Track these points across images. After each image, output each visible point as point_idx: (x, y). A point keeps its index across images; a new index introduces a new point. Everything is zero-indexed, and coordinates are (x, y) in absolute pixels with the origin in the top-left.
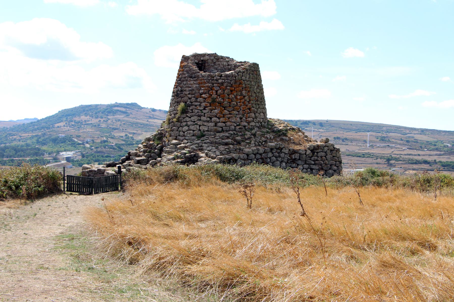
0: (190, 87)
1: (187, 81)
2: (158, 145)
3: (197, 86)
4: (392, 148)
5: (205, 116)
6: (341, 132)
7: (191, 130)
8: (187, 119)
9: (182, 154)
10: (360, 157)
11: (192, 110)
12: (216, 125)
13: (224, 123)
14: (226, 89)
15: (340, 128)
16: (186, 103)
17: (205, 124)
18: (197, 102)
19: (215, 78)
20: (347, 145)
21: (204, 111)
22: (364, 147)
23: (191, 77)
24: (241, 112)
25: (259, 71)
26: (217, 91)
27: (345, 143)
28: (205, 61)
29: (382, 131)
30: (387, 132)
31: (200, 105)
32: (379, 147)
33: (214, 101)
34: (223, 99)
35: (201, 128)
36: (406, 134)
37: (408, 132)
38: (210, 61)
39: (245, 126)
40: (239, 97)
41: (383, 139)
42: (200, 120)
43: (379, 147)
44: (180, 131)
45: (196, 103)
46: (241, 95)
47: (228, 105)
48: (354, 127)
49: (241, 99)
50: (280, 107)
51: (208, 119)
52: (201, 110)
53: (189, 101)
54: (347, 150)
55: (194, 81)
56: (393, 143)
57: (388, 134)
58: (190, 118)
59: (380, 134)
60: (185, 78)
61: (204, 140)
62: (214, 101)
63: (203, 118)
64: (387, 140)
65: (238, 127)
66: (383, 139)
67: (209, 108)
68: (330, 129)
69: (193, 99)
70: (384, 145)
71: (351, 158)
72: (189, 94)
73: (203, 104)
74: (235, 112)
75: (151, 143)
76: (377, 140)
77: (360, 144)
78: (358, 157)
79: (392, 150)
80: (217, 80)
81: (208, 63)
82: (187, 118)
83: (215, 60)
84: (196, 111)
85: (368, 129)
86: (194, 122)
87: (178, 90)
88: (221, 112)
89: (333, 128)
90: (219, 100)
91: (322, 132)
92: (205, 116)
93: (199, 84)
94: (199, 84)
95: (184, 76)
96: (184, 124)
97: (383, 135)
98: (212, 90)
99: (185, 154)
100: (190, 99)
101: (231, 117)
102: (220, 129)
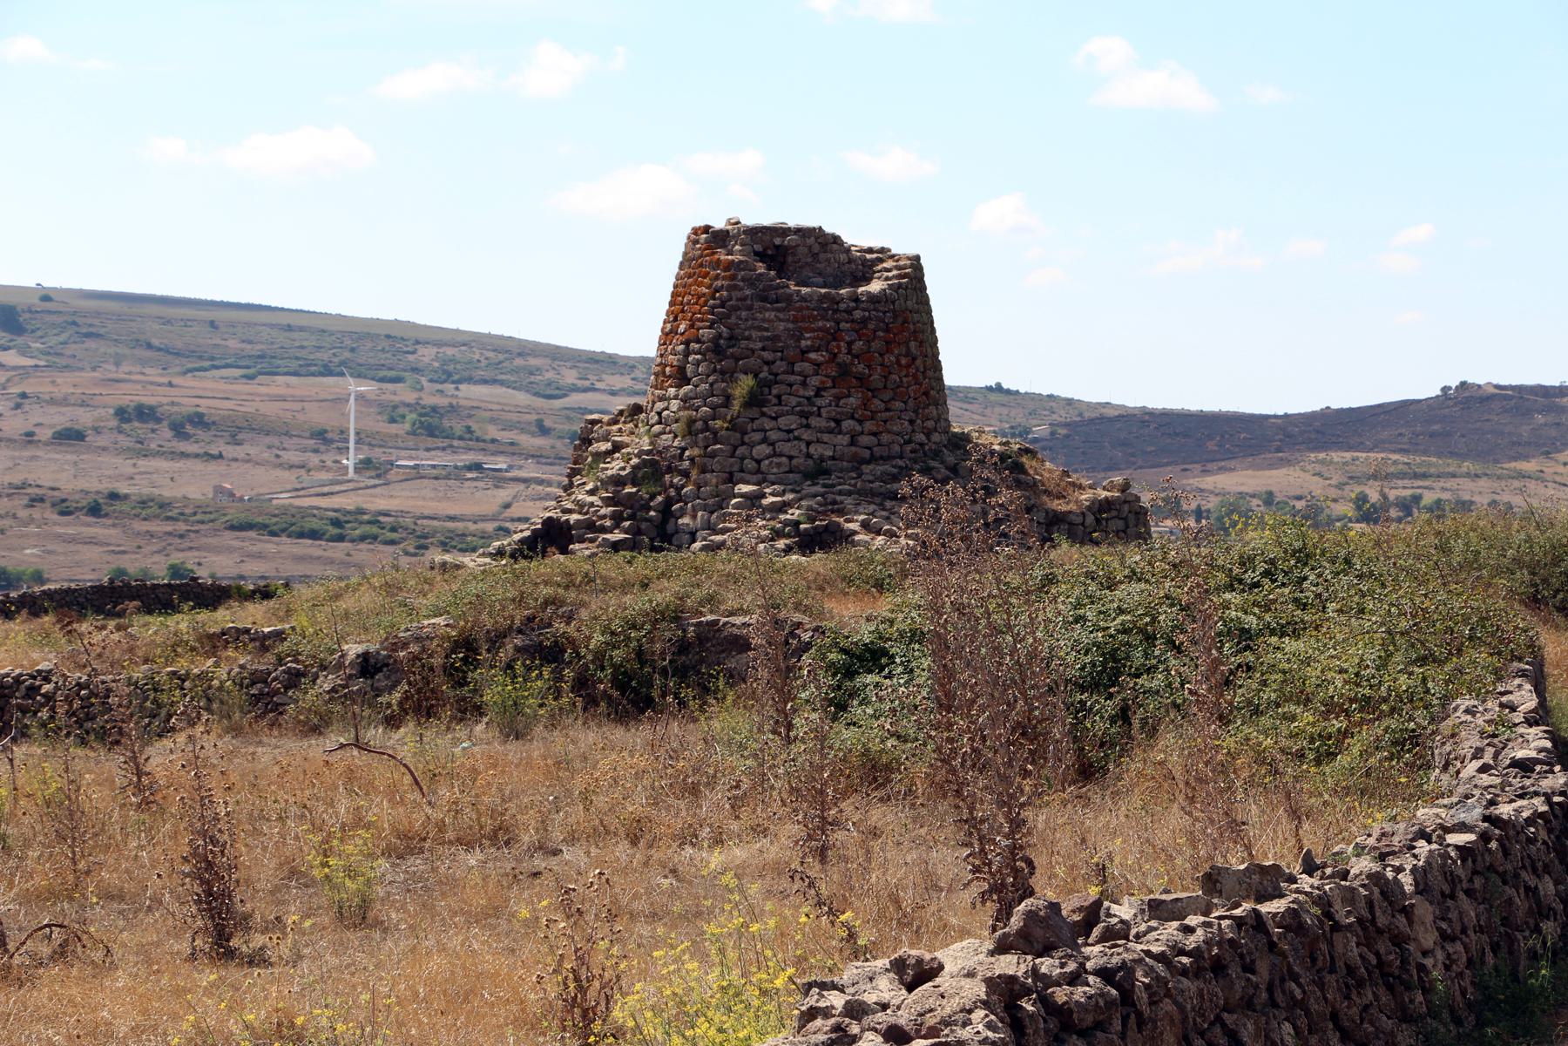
0: (767, 330)
1: (750, 308)
2: (653, 497)
3: (791, 326)
4: (499, 478)
5: (819, 415)
6: (153, 374)
7: (781, 455)
8: (768, 424)
9: (786, 523)
10: (314, 535)
11: (779, 397)
12: (853, 443)
13: (875, 434)
14: (875, 337)
15: (137, 343)
16: (756, 376)
17: (826, 437)
18: (793, 373)
19: (843, 306)
20: (213, 457)
21: (819, 402)
22: (324, 476)
23: (765, 299)
24: (911, 403)
26: (850, 344)
27: (192, 448)
28: (787, 248)
29: (415, 370)
30: (447, 374)
31: (804, 384)
32: (417, 474)
33: (844, 371)
34: (869, 367)
35: (812, 450)
36: (563, 392)
37: (570, 377)
38: (802, 250)
39: (922, 445)
40: (904, 361)
41: (432, 426)
42: (808, 426)
43: (417, 474)
44: (743, 459)
45: (792, 378)
46: (908, 354)
47: (881, 385)
48: (233, 344)
49: (908, 366)
50: (979, 348)
51: (833, 424)
52: (808, 399)
53: (766, 368)
54: (219, 490)
55: (778, 310)
56: (496, 448)
57: (449, 387)
58: (775, 419)
60: (743, 299)
61: (833, 486)
62: (844, 371)
63: (814, 421)
64: (458, 429)
65: (908, 448)
66: (432, 426)
67: (834, 391)
68: (71, 349)
69: (780, 366)
71: (259, 547)
72: (763, 349)
73: (814, 381)
74: (899, 405)
75: (629, 490)
76: (394, 429)
77: (292, 456)
78: (301, 535)
79: (504, 495)
80: (849, 312)
81: (794, 254)
82: (765, 420)
83: (816, 248)
84: (793, 401)
85: (325, 356)
86: (789, 431)
87: (720, 336)
88: (865, 405)
89: (91, 344)
90: (804, 343)
91: (24, 373)
92: (819, 415)
93: (795, 320)
94: (795, 320)
95: (735, 294)
96: (758, 436)
97: (429, 400)
98: (835, 339)
99: (797, 523)
100: (767, 363)
101: (891, 418)
102: (867, 454)
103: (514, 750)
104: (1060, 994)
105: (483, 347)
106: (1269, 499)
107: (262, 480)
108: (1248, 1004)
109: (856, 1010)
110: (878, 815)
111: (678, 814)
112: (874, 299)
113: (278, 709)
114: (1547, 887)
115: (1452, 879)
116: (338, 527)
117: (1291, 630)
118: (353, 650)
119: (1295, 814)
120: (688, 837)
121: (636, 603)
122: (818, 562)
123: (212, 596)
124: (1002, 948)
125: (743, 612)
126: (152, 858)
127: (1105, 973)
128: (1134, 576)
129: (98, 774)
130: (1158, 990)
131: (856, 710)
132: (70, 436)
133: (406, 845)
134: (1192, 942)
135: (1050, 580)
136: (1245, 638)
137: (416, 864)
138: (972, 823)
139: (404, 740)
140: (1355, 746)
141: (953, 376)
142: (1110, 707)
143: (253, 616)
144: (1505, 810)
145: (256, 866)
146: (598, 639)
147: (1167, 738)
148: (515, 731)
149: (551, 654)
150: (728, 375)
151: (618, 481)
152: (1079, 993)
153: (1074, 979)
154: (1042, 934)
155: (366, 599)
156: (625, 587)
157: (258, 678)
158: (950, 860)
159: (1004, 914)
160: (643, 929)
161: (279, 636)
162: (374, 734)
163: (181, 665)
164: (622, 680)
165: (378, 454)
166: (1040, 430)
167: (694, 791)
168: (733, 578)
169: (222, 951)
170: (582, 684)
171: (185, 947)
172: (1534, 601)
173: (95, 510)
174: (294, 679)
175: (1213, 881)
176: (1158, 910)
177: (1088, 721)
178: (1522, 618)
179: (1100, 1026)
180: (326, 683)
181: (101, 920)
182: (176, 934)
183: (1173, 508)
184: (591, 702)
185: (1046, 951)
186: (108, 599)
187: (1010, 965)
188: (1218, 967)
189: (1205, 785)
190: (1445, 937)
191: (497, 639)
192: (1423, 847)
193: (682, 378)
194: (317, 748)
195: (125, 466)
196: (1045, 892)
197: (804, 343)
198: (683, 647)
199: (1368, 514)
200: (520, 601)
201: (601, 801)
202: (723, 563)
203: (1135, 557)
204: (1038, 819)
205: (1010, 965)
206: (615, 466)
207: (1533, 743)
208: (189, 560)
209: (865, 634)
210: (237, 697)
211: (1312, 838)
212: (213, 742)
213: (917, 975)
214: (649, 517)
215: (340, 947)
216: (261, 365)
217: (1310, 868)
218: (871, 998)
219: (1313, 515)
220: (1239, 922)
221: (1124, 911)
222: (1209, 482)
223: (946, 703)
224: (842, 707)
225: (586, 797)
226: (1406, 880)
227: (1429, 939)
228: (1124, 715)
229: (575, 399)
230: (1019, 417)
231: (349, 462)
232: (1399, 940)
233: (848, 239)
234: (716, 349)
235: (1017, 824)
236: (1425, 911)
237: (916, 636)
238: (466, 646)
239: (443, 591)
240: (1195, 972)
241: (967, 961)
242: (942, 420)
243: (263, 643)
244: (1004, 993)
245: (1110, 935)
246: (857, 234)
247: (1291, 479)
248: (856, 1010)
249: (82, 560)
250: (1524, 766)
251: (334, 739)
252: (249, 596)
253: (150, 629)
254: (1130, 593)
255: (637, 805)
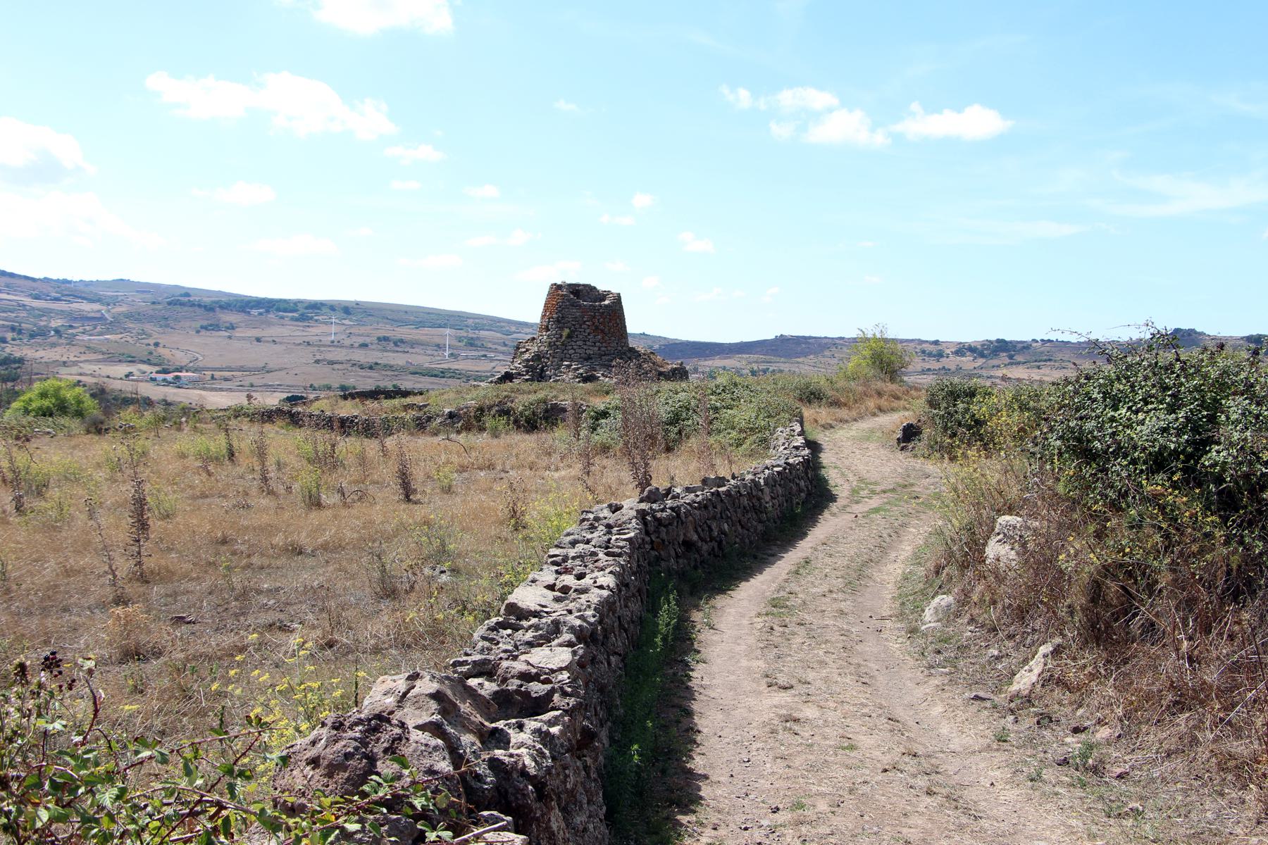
4: (492, 360)
10: (436, 376)
25: (46, 280)
32: (467, 358)
33: (597, 328)
37: (513, 329)
41: (471, 343)
43: (467, 358)
50: (636, 323)
59: (463, 333)
62: (597, 328)
66: (471, 343)
70: (474, 353)
77: (429, 352)
79: (493, 364)
90: (585, 322)
103: (495, 441)
104: (658, 515)
105: (398, 311)
106: (724, 368)
107: (420, 359)
108: (714, 518)
109: (597, 519)
110: (605, 462)
111: (544, 461)
112: (606, 306)
113: (424, 428)
114: (802, 483)
115: (775, 481)
116: (443, 374)
117: (730, 407)
118: (447, 410)
119: (730, 462)
120: (548, 468)
121: (533, 397)
122: (589, 385)
123: (405, 394)
124: (641, 501)
125: (565, 401)
126: (387, 472)
127: (672, 509)
128: (683, 391)
129: (372, 446)
130: (688, 514)
131: (599, 430)
132: (364, 346)
133: (462, 469)
134: (698, 499)
135: (658, 391)
136: (716, 409)
137: (465, 475)
138: (634, 464)
139: (462, 438)
140: (748, 442)
141: (630, 330)
142: (676, 430)
143: (418, 400)
144: (791, 461)
145: (418, 474)
146: (521, 408)
147: (693, 440)
148: (495, 435)
149: (505, 412)
150: (562, 329)
151: (528, 360)
152: (664, 514)
153: (663, 510)
154: (653, 497)
155: (452, 395)
156: (529, 393)
157: (419, 418)
158: (627, 475)
159: (642, 492)
160: (534, 495)
161: (425, 406)
162: (453, 436)
163: (396, 414)
164: (528, 421)
165: (455, 352)
166: (657, 347)
167: (550, 454)
168: (563, 391)
169: (408, 499)
170: (516, 422)
171: (396, 498)
172: (801, 400)
173: (371, 368)
174: (429, 419)
175: (705, 481)
176: (688, 490)
177: (670, 434)
178: (798, 404)
179: (670, 524)
180: (439, 420)
181: (372, 489)
182: (394, 494)
183: (696, 371)
184: (519, 427)
185: (654, 502)
186: (374, 394)
187: (644, 506)
188: (706, 507)
189: (704, 453)
190: (773, 498)
191: (490, 408)
192: (767, 472)
193: (548, 330)
194: (436, 440)
195: (380, 354)
196: (654, 484)
197: (585, 322)
198: (547, 411)
199: (753, 373)
200: (497, 396)
201: (521, 457)
202: (559, 386)
203: (684, 385)
204: (653, 463)
205: (644, 506)
206: (526, 356)
207: (799, 441)
208: (398, 383)
209: (602, 407)
210: (413, 424)
211: (735, 470)
212: (404, 437)
213: (615, 509)
214: (537, 372)
215: (441, 499)
216: (420, 324)
217: (734, 477)
218: (601, 515)
219: (738, 372)
220: (713, 494)
221: (678, 490)
222: (707, 363)
223: (625, 427)
224: (595, 429)
225: (517, 455)
226: (762, 481)
227: (768, 499)
228: (680, 432)
229: (515, 336)
230: (650, 343)
231: (446, 354)
232: (759, 499)
233: (598, 288)
234: (558, 321)
235: (647, 465)
236: (767, 490)
237: (617, 408)
238: (481, 409)
239: (474, 393)
240: (699, 508)
241: (631, 504)
242: (626, 343)
243: (420, 408)
244: (642, 515)
245: (674, 497)
246: (601, 287)
247: (730, 362)
248: (597, 519)
249: (368, 384)
250: (797, 448)
251: (441, 437)
252: (415, 394)
253: (387, 404)
254: (682, 396)
255: (532, 458)
